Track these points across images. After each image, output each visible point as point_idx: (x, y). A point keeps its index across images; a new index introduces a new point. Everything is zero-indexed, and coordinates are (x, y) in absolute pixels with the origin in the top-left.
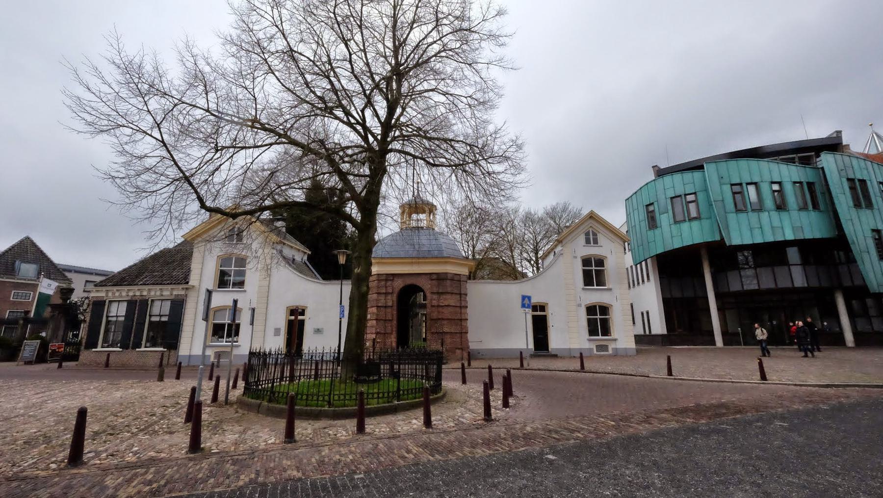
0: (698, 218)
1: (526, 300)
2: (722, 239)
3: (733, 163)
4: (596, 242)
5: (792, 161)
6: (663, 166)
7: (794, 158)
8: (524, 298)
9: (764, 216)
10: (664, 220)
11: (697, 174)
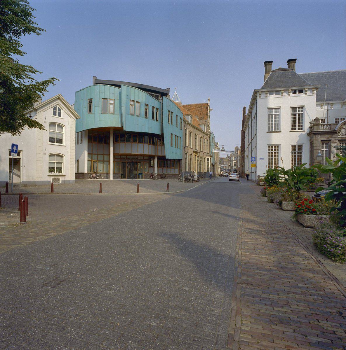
0: (114, 114)
1: (15, 148)
2: (122, 127)
3: (137, 90)
4: (60, 115)
5: (152, 95)
6: (99, 78)
7: (153, 95)
8: (13, 145)
9: (140, 118)
10: (97, 109)
11: (117, 89)
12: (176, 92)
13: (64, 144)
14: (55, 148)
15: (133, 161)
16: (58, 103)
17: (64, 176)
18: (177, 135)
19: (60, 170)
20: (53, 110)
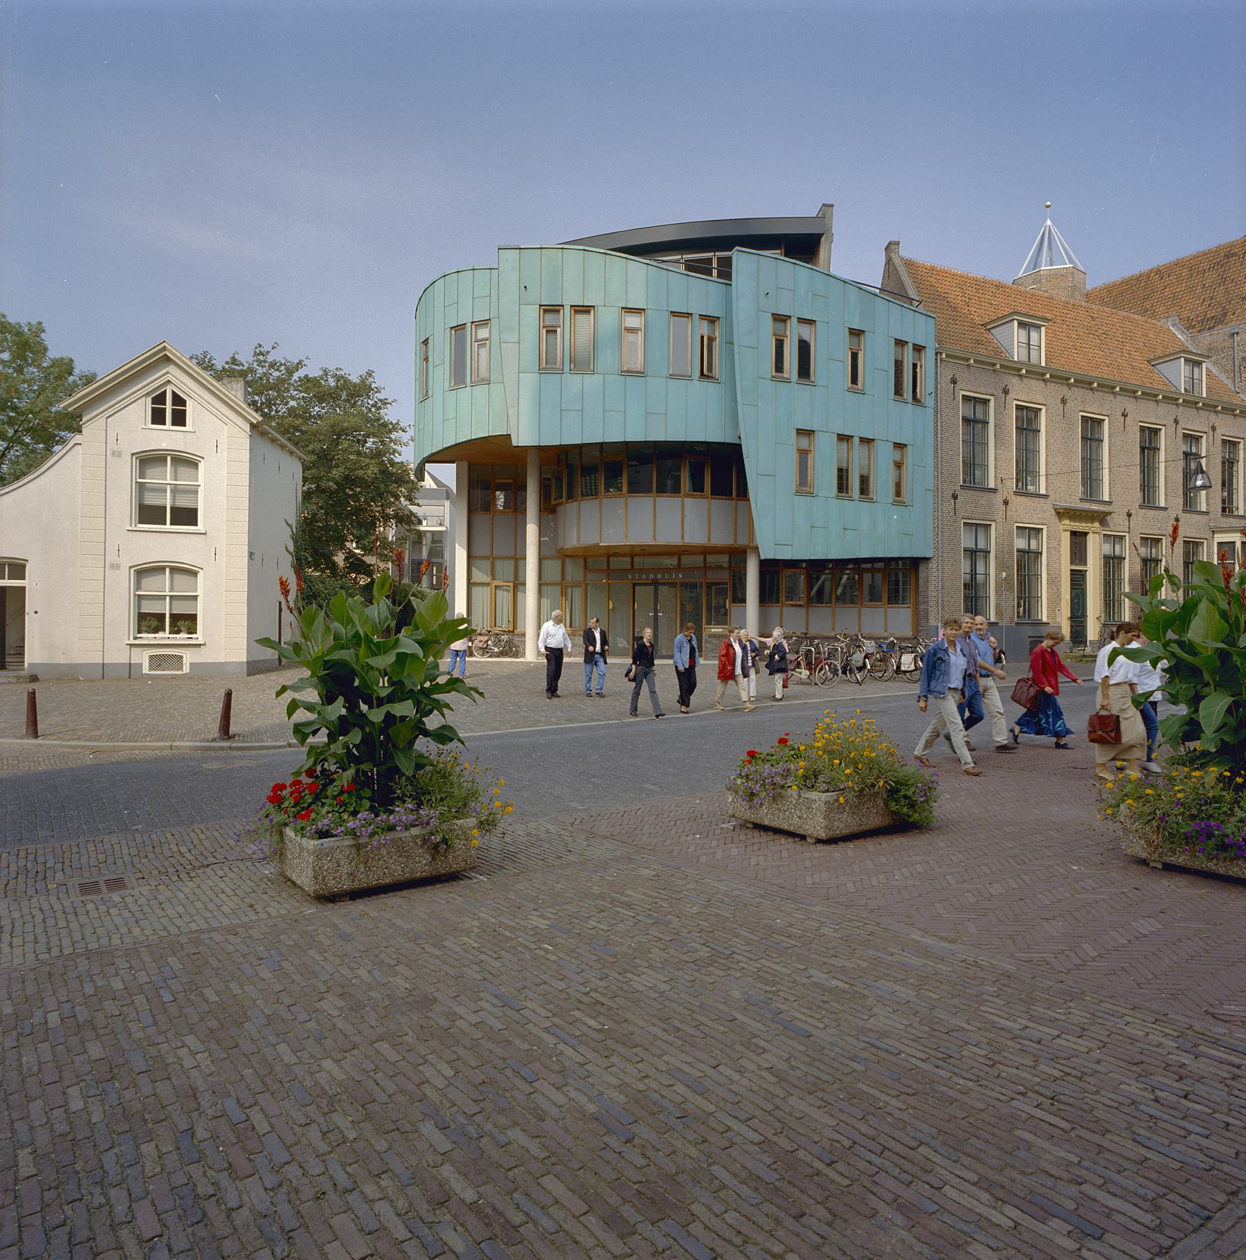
4: (180, 419)
12: (1049, 223)
13: (200, 527)
14: (165, 544)
15: (659, 576)
16: (169, 377)
17: (199, 645)
18: (857, 430)
19: (185, 622)
20: (150, 406)
